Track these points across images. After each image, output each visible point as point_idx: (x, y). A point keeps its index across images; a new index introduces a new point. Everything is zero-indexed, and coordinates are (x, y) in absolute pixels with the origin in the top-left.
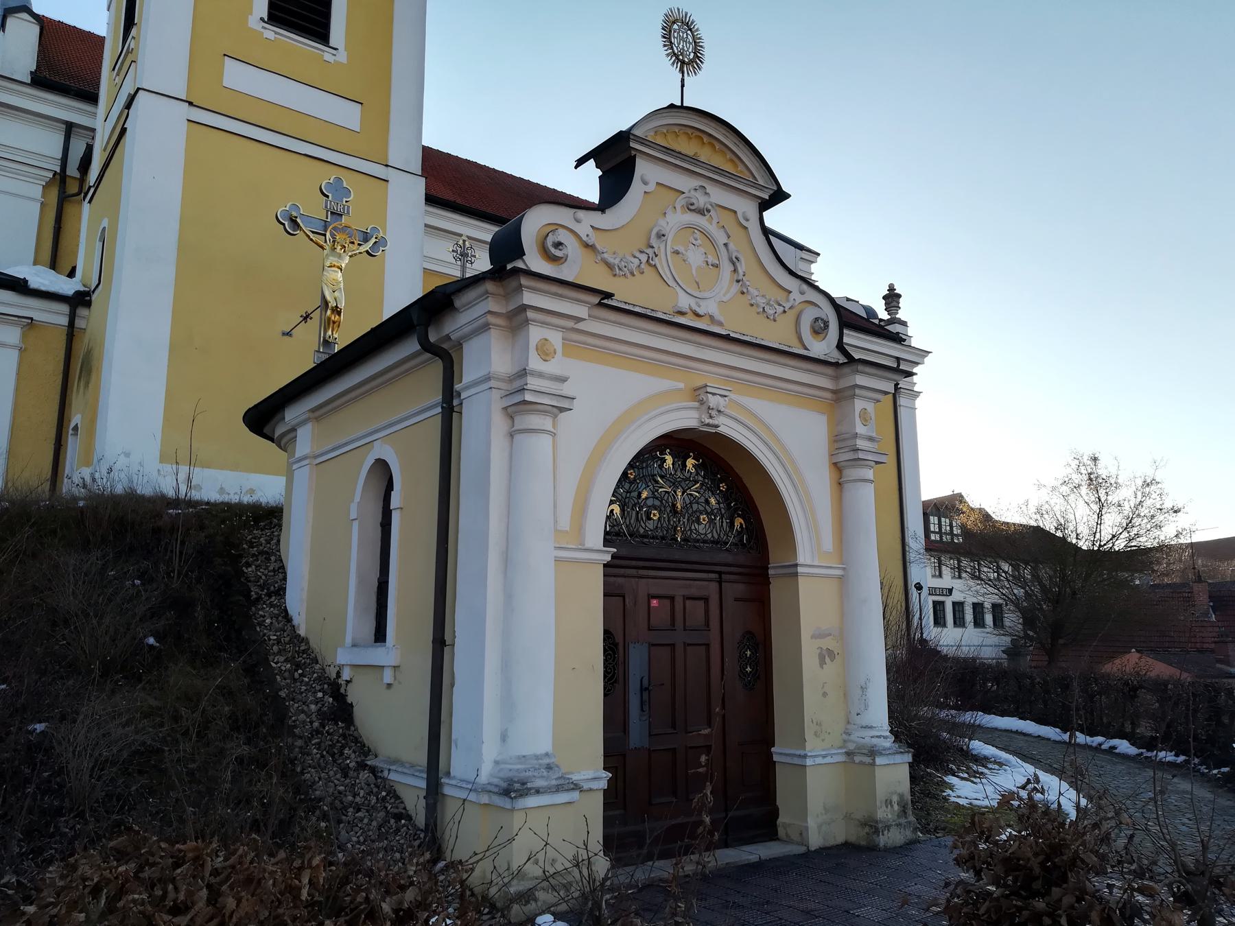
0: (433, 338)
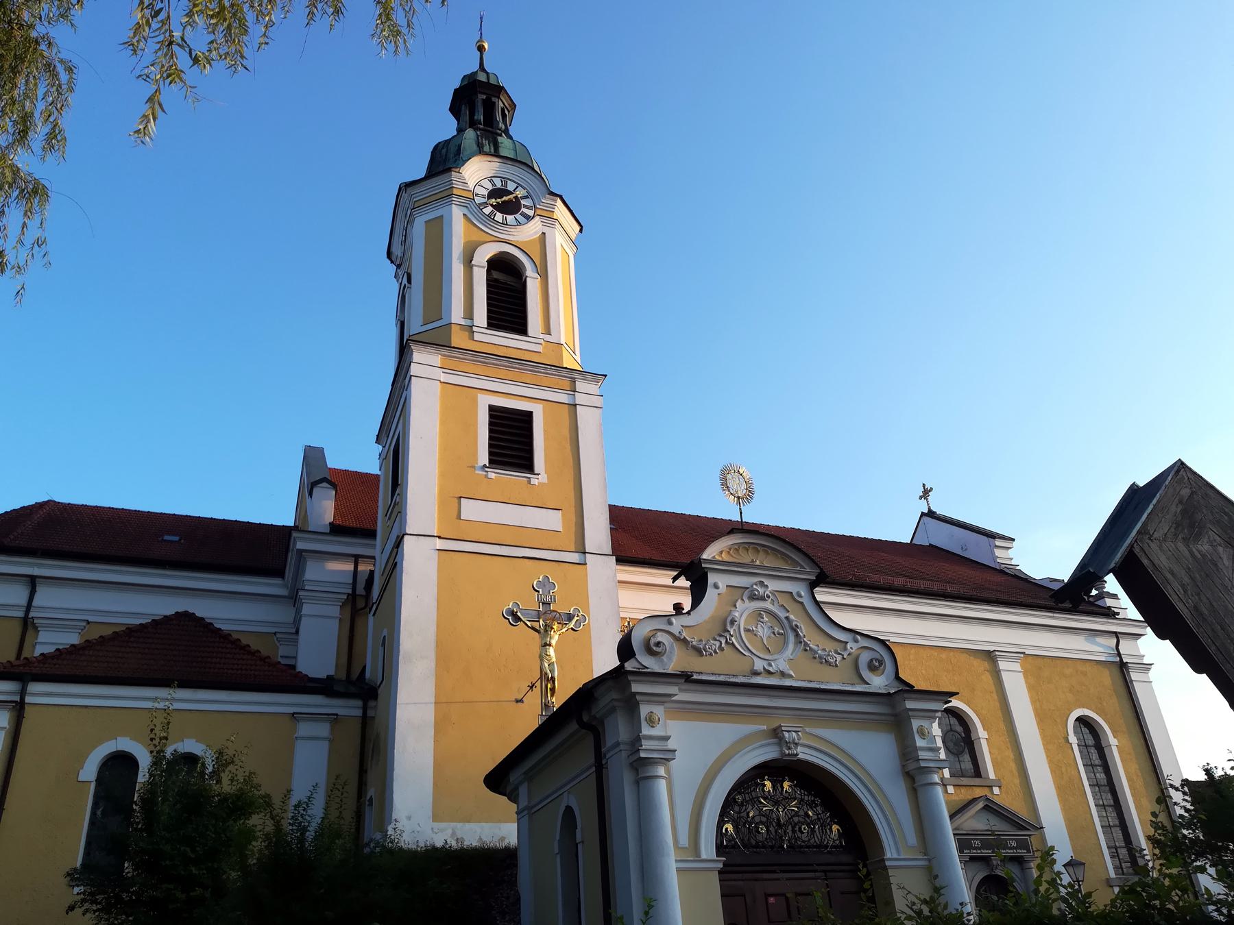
0: (585, 718)
